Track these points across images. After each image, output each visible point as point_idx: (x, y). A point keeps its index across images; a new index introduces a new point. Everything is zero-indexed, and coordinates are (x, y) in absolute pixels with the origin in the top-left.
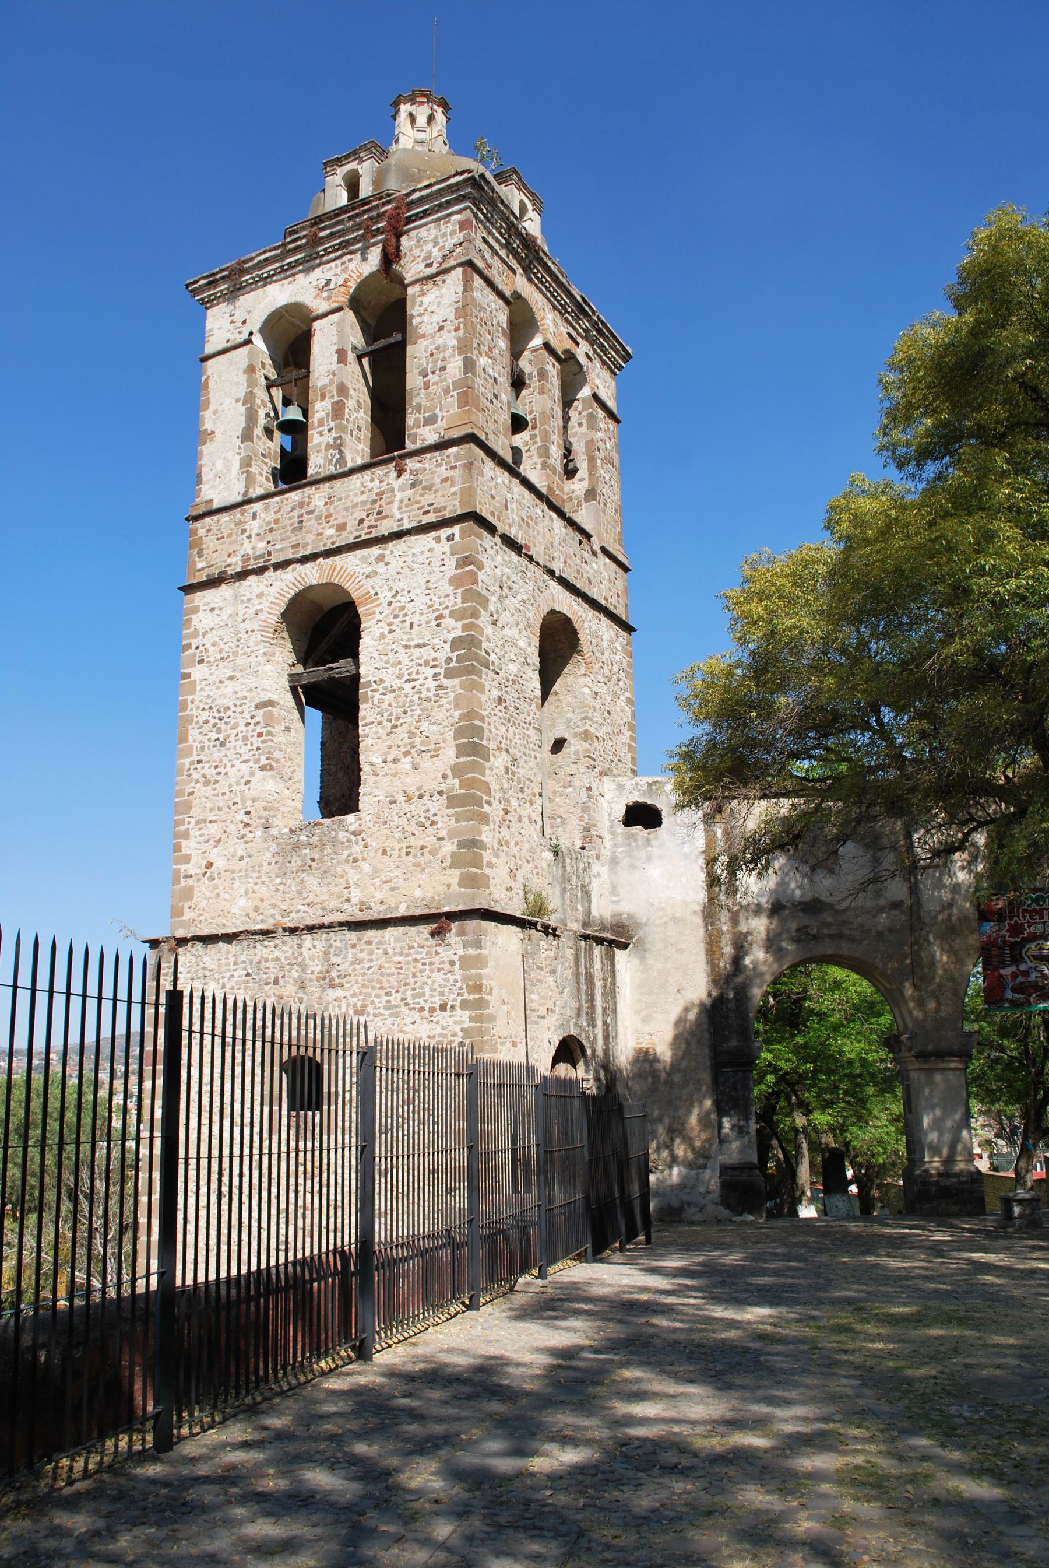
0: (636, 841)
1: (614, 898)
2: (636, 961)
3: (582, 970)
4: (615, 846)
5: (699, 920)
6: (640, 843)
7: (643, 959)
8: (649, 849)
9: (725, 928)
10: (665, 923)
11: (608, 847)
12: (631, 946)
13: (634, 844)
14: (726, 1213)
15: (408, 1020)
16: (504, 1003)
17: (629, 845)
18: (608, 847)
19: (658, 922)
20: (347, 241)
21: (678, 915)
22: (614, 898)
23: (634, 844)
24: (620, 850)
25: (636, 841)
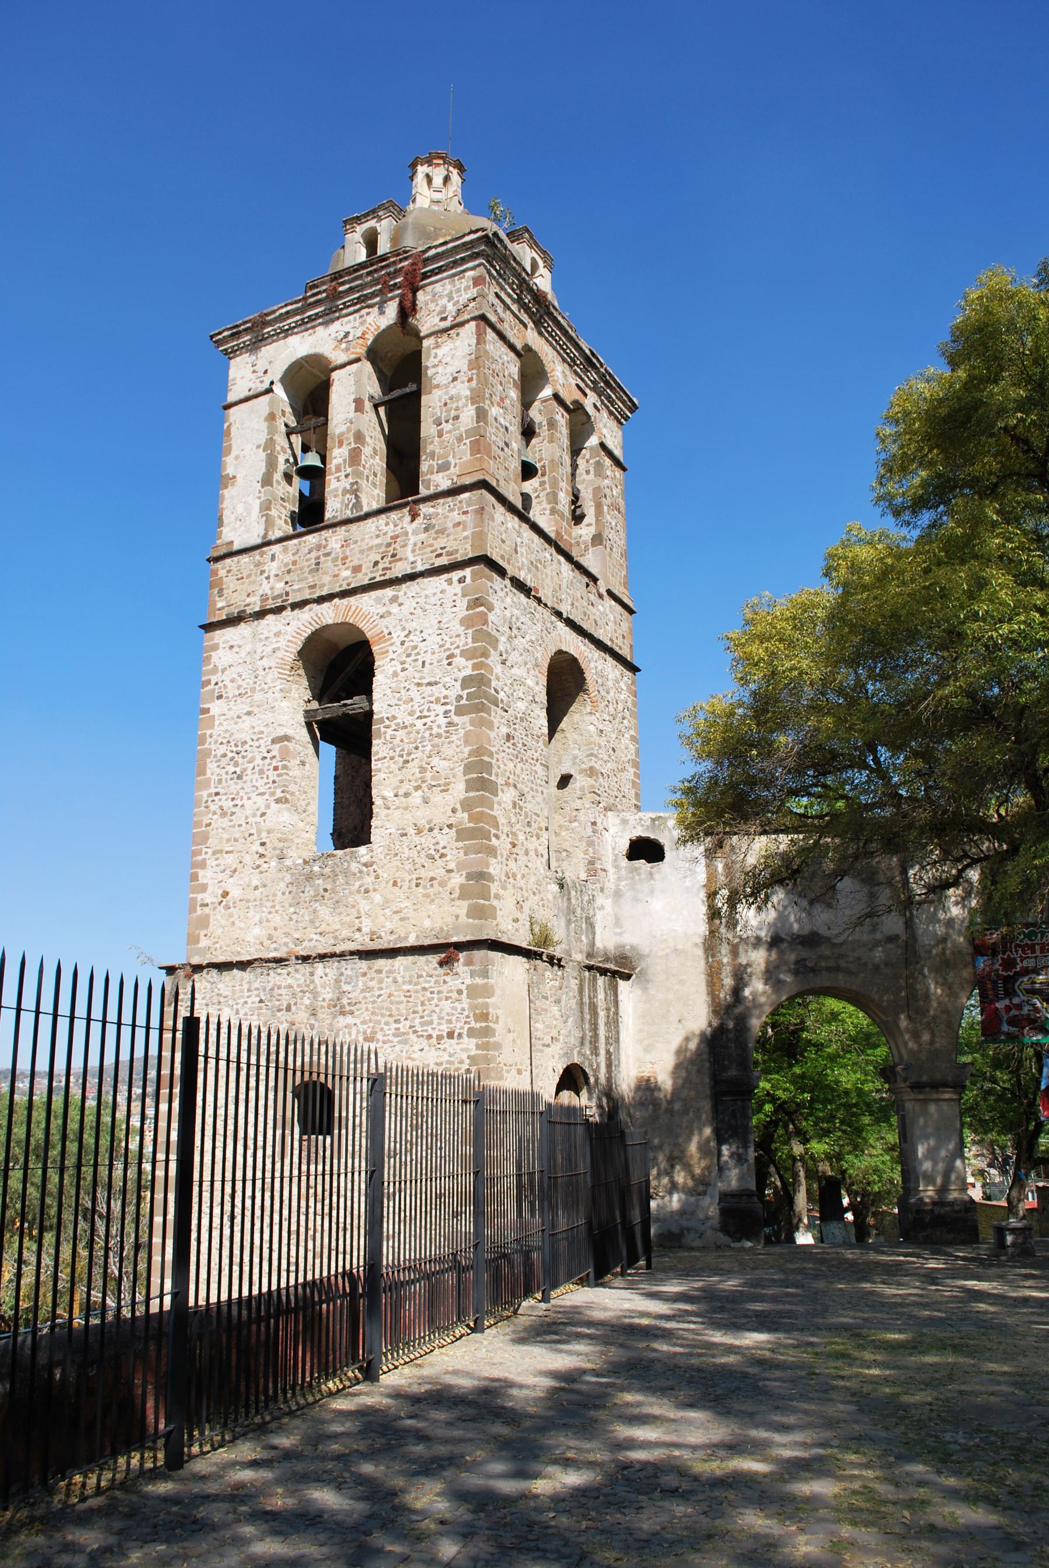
0: (639, 874)
1: (618, 930)
2: (639, 992)
3: (586, 1000)
4: (619, 879)
5: (700, 952)
6: (643, 876)
7: (645, 989)
8: (652, 882)
9: (725, 960)
10: (667, 954)
11: (612, 881)
12: (634, 977)
13: (637, 878)
14: (724, 1239)
15: (417, 1047)
16: (509, 1031)
17: (633, 878)
18: (612, 881)
19: (660, 953)
20: (365, 295)
21: (679, 947)
22: (618, 930)
23: (637, 878)
24: (623, 883)
25: (639, 874)
